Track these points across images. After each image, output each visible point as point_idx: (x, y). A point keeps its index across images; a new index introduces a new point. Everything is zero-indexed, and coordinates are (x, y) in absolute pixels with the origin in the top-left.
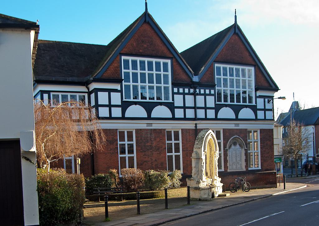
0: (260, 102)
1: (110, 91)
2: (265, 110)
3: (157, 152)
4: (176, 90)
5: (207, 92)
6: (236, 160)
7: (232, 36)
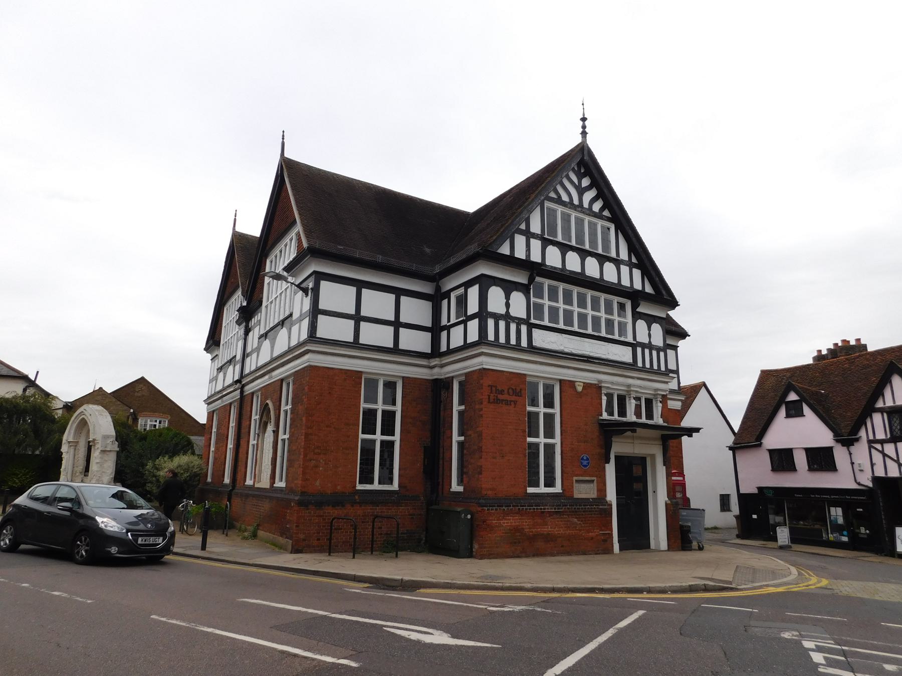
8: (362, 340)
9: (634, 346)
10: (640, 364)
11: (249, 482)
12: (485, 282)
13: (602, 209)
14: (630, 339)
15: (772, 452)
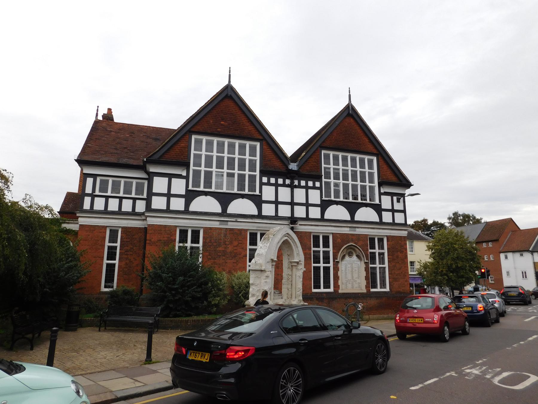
0: (386, 202)
1: (170, 176)
2: (393, 211)
3: (233, 261)
4: (265, 180)
5: (310, 184)
6: (353, 277)
7: (345, 118)
15: (80, 225)
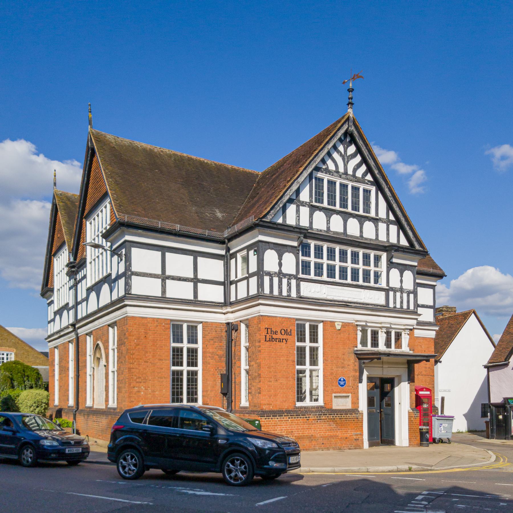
8: (168, 295)
9: (387, 291)
10: (391, 305)
11: (89, 403)
12: (259, 248)
13: (365, 174)
14: (384, 285)
